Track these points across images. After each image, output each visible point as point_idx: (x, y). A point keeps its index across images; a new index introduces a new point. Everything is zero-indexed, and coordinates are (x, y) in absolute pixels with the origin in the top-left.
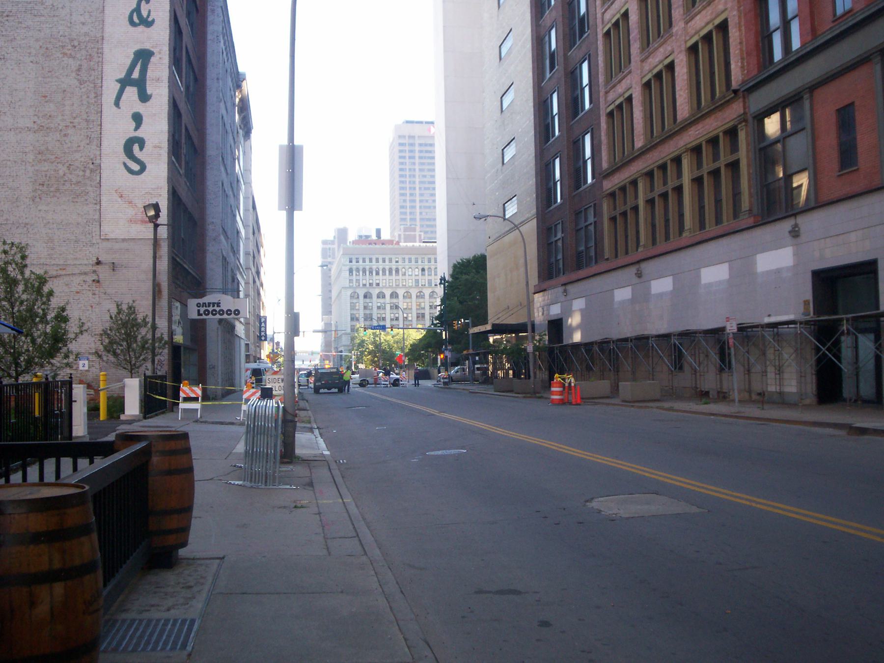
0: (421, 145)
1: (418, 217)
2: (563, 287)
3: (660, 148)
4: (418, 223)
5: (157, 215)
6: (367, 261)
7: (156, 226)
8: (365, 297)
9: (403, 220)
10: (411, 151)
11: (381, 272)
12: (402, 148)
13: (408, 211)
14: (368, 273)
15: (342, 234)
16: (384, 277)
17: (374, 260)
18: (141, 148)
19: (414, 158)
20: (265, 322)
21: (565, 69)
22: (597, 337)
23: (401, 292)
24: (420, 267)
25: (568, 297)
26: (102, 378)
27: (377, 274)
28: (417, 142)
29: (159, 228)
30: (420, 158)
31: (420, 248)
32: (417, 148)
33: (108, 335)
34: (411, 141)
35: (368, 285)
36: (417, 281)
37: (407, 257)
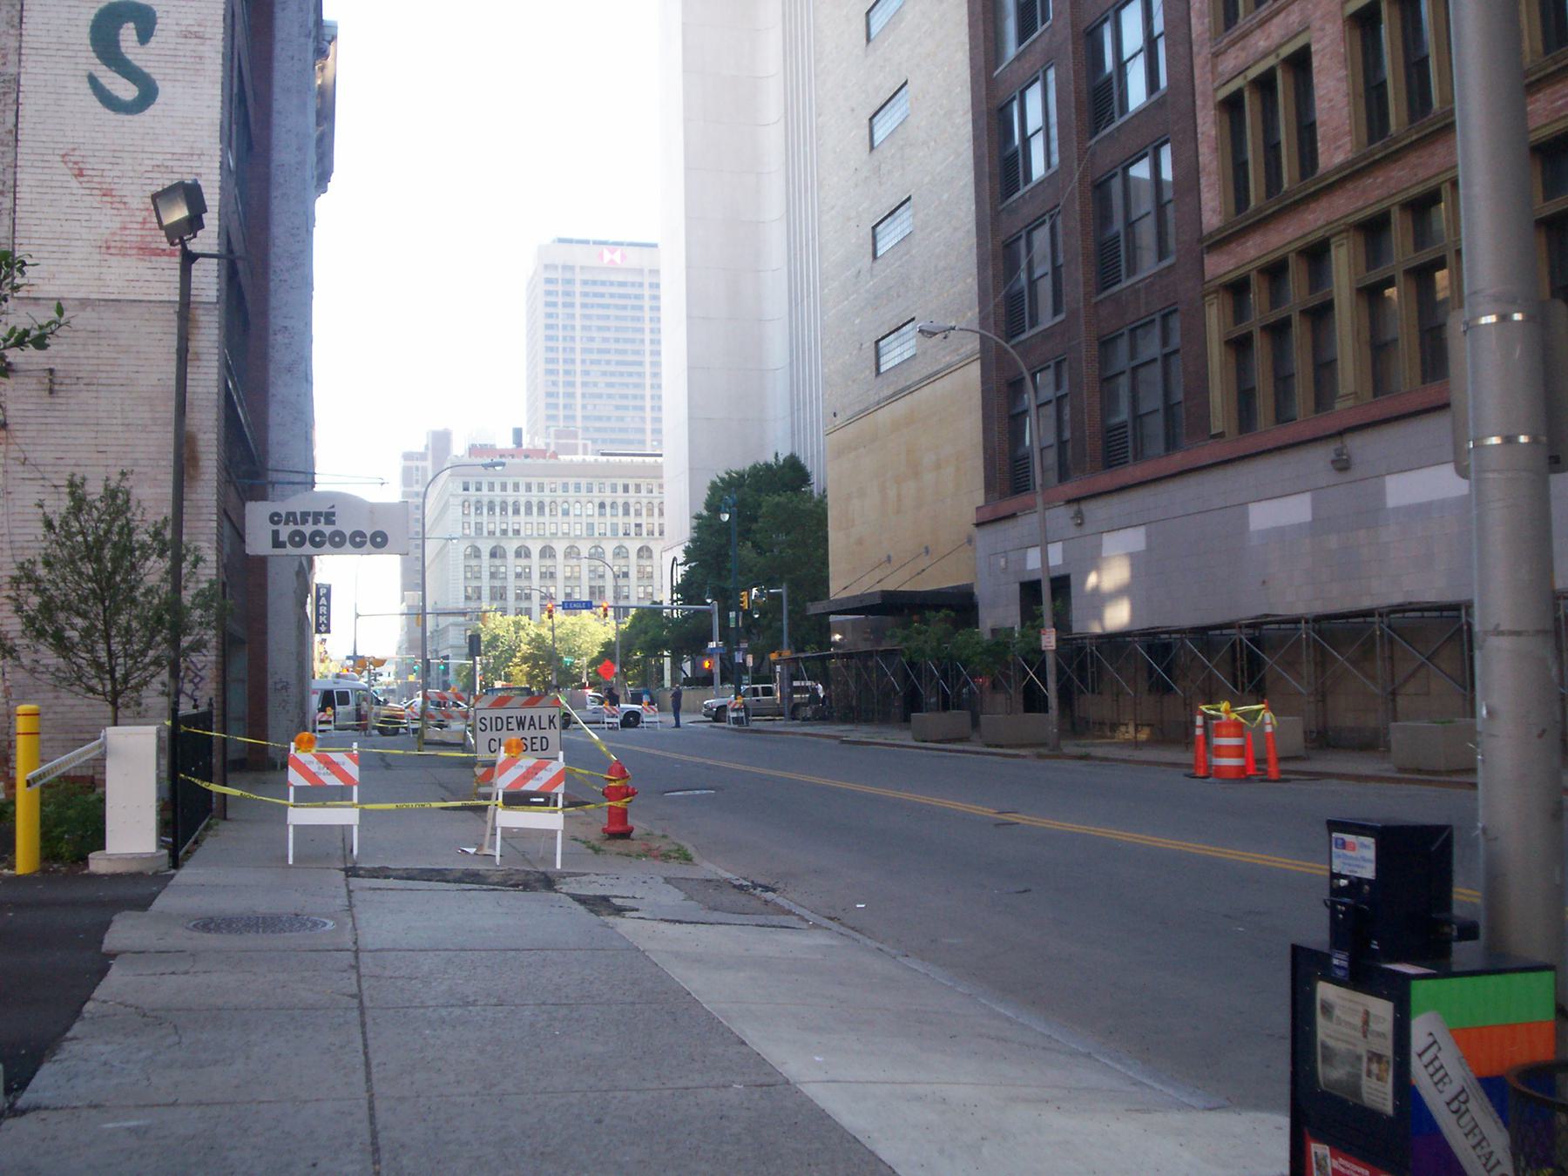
0: (585, 283)
1: (579, 413)
2: (1074, 507)
3: (1413, 158)
4: (579, 423)
5: (194, 223)
6: (497, 487)
7: (189, 258)
8: (493, 555)
9: (550, 418)
10: (567, 294)
11: (522, 510)
12: (551, 287)
13: (561, 401)
14: (498, 510)
15: (441, 441)
16: (529, 519)
17: (510, 487)
18: (145, 36)
19: (572, 305)
20: (328, 596)
21: (1074, 25)
22: (1186, 613)
23: (560, 547)
24: (597, 501)
25: (1087, 529)
26: (22, 724)
27: (516, 512)
28: (579, 277)
29: (197, 269)
30: (584, 306)
31: (596, 464)
32: (578, 288)
33: (38, 581)
34: (568, 276)
35: (498, 534)
36: (591, 526)
37: (572, 481)
